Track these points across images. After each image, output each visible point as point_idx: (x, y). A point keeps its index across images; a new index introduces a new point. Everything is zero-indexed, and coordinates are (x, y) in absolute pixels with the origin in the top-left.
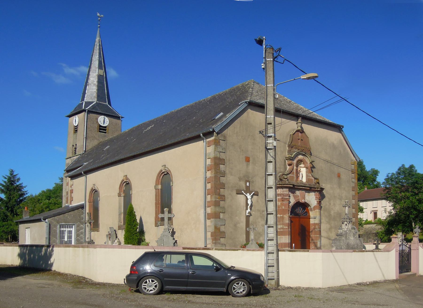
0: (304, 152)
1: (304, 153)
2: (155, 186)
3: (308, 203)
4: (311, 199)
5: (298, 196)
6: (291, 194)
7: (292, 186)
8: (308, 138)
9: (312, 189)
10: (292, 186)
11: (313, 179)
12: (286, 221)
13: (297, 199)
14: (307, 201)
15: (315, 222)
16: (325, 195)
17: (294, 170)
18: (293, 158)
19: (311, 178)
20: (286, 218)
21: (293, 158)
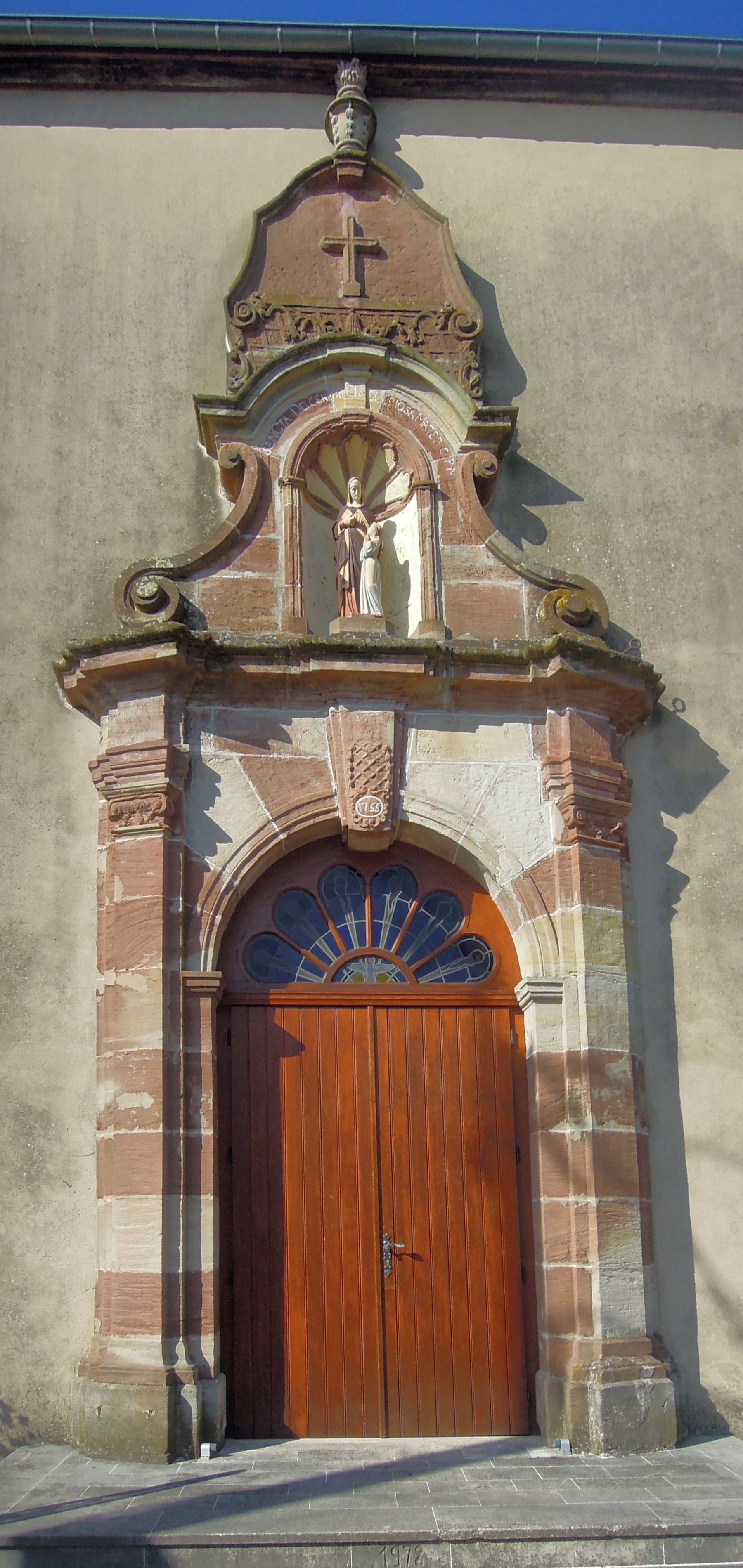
0: (371, 343)
1: (380, 353)
2: (562, 834)
3: (446, 832)
4: (491, 791)
5: (318, 768)
6: (226, 753)
7: (173, 652)
8: (441, 220)
9: (474, 676)
10: (173, 652)
11: (515, 592)
12: (145, 1038)
13: (303, 796)
14: (425, 810)
15: (206, 1194)
16: (716, 754)
17: (274, 528)
18: (241, 413)
19: (485, 582)
20: (139, 995)
21: (241, 413)
